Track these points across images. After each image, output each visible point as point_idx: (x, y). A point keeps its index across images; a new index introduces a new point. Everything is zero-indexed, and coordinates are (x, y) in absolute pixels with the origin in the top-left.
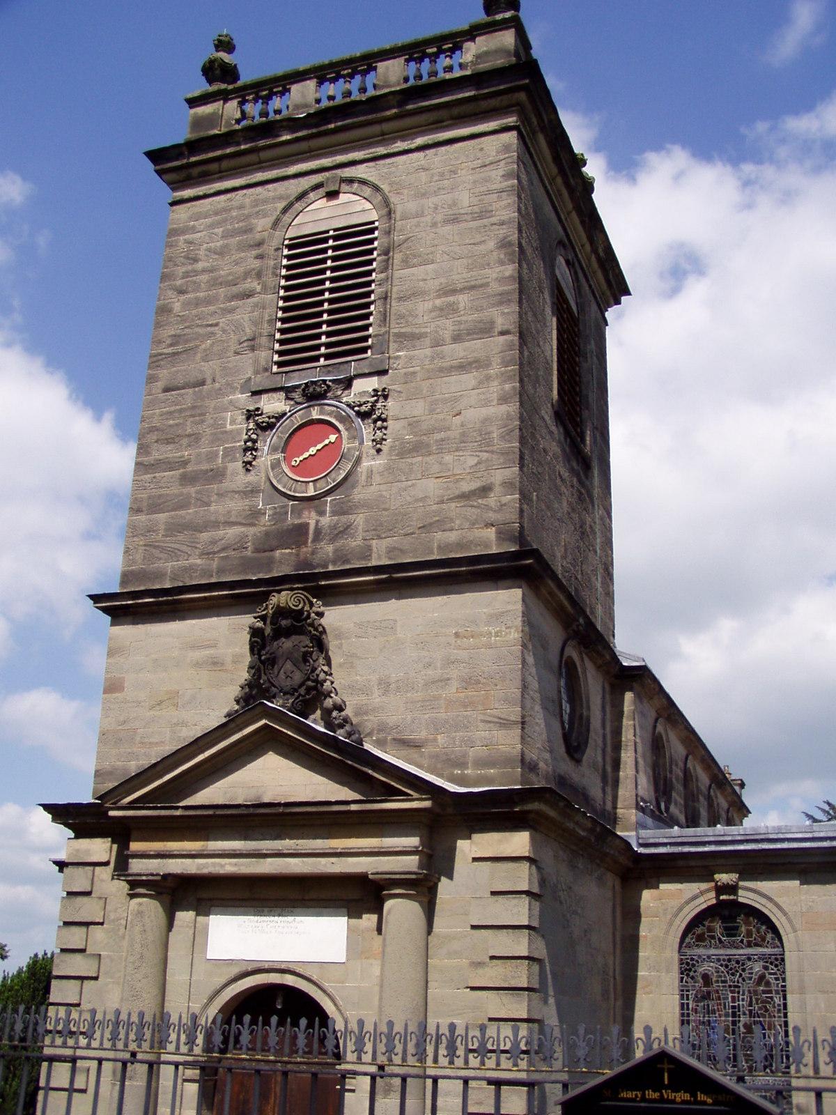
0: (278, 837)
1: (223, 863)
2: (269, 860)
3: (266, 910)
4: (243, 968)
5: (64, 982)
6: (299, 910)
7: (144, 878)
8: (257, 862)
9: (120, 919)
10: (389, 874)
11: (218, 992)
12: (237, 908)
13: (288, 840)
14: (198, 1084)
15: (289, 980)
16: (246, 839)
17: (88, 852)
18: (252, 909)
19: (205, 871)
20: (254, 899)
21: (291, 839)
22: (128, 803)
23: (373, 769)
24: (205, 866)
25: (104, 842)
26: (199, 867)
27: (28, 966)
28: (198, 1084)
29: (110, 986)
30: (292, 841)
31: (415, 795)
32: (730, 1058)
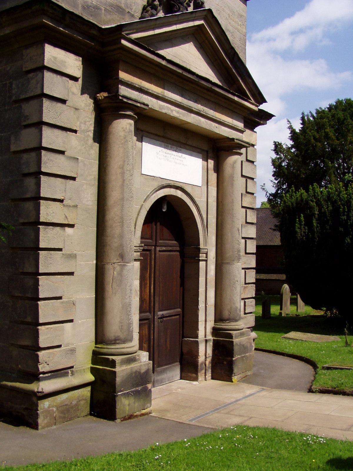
0: (196, 102)
1: (172, 109)
2: (193, 115)
3: (170, 146)
4: (165, 183)
5: (53, 179)
6: (183, 150)
7: (139, 105)
8: (187, 113)
9: (89, 131)
10: (241, 141)
11: (148, 197)
12: (152, 139)
13: (200, 105)
14: (139, 262)
15: (179, 194)
16: (182, 96)
17: (63, 62)
18: (163, 144)
19: (164, 111)
20: (163, 137)
21: (202, 105)
22: (136, 39)
23: (242, 79)
24: (163, 107)
25: (76, 59)
26: (160, 106)
27: (274, 168)
28: (139, 262)
29: (85, 187)
30: (202, 106)
31: (253, 101)
32: (306, 232)
